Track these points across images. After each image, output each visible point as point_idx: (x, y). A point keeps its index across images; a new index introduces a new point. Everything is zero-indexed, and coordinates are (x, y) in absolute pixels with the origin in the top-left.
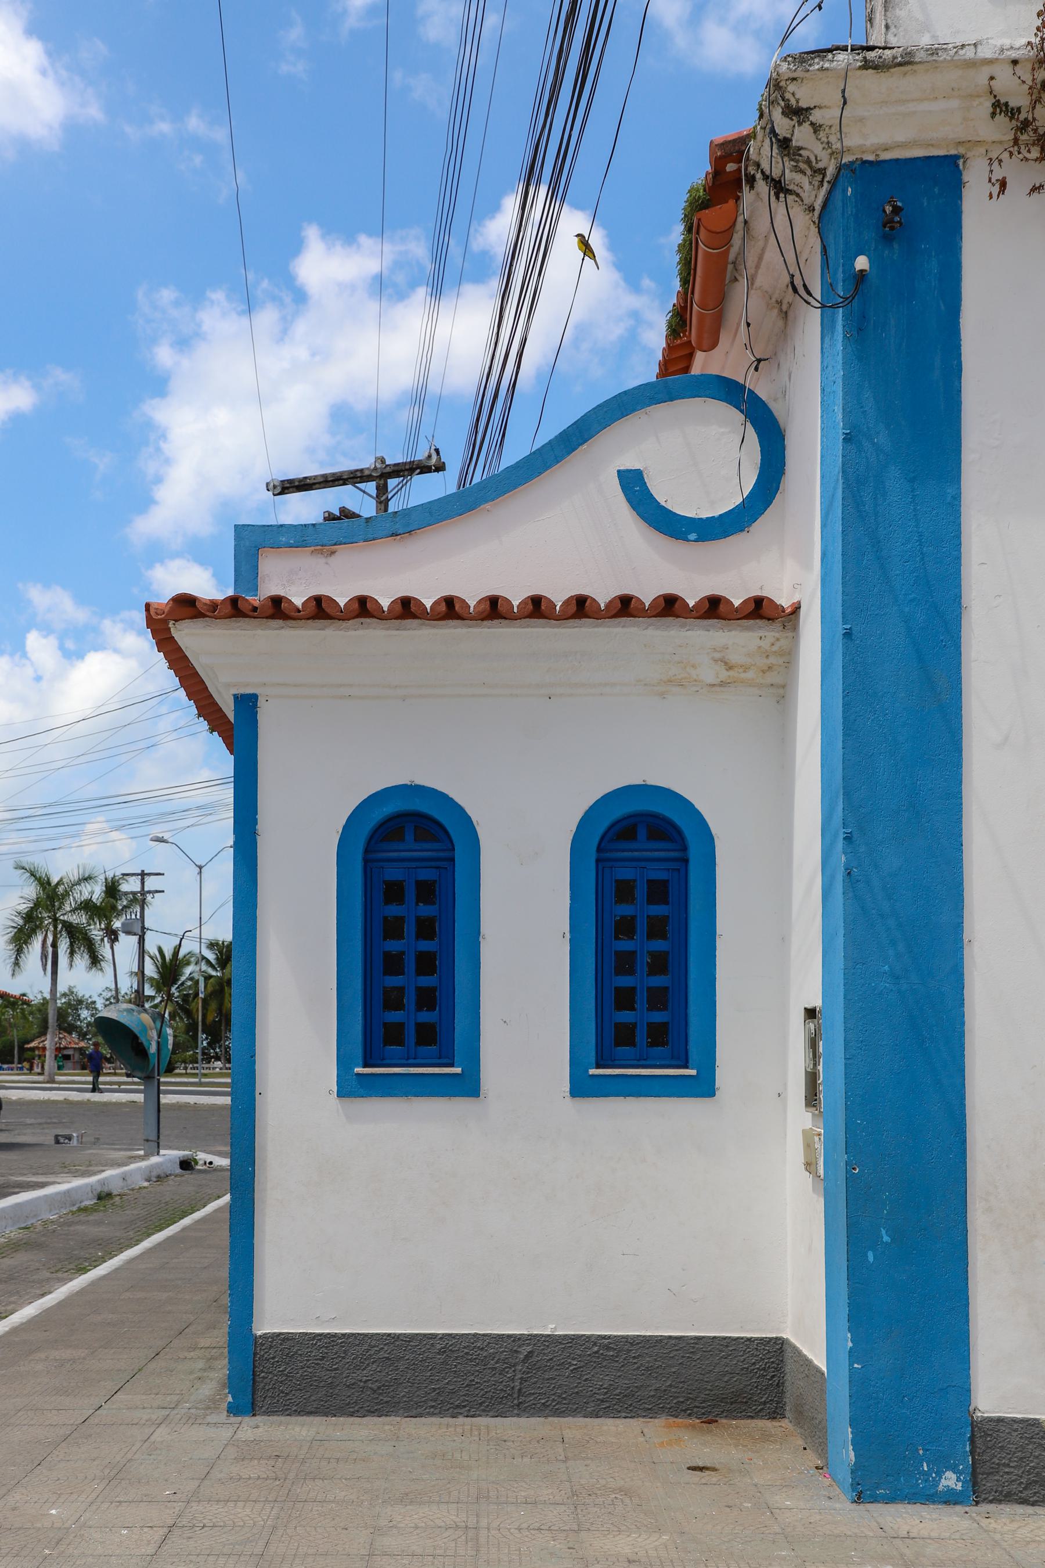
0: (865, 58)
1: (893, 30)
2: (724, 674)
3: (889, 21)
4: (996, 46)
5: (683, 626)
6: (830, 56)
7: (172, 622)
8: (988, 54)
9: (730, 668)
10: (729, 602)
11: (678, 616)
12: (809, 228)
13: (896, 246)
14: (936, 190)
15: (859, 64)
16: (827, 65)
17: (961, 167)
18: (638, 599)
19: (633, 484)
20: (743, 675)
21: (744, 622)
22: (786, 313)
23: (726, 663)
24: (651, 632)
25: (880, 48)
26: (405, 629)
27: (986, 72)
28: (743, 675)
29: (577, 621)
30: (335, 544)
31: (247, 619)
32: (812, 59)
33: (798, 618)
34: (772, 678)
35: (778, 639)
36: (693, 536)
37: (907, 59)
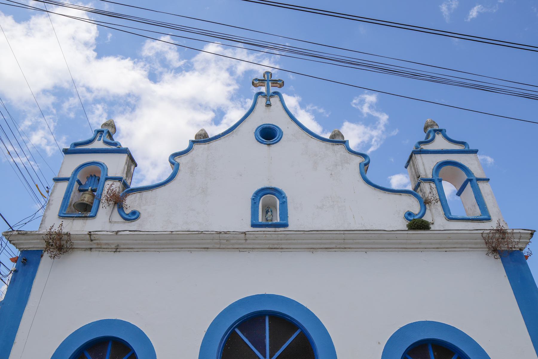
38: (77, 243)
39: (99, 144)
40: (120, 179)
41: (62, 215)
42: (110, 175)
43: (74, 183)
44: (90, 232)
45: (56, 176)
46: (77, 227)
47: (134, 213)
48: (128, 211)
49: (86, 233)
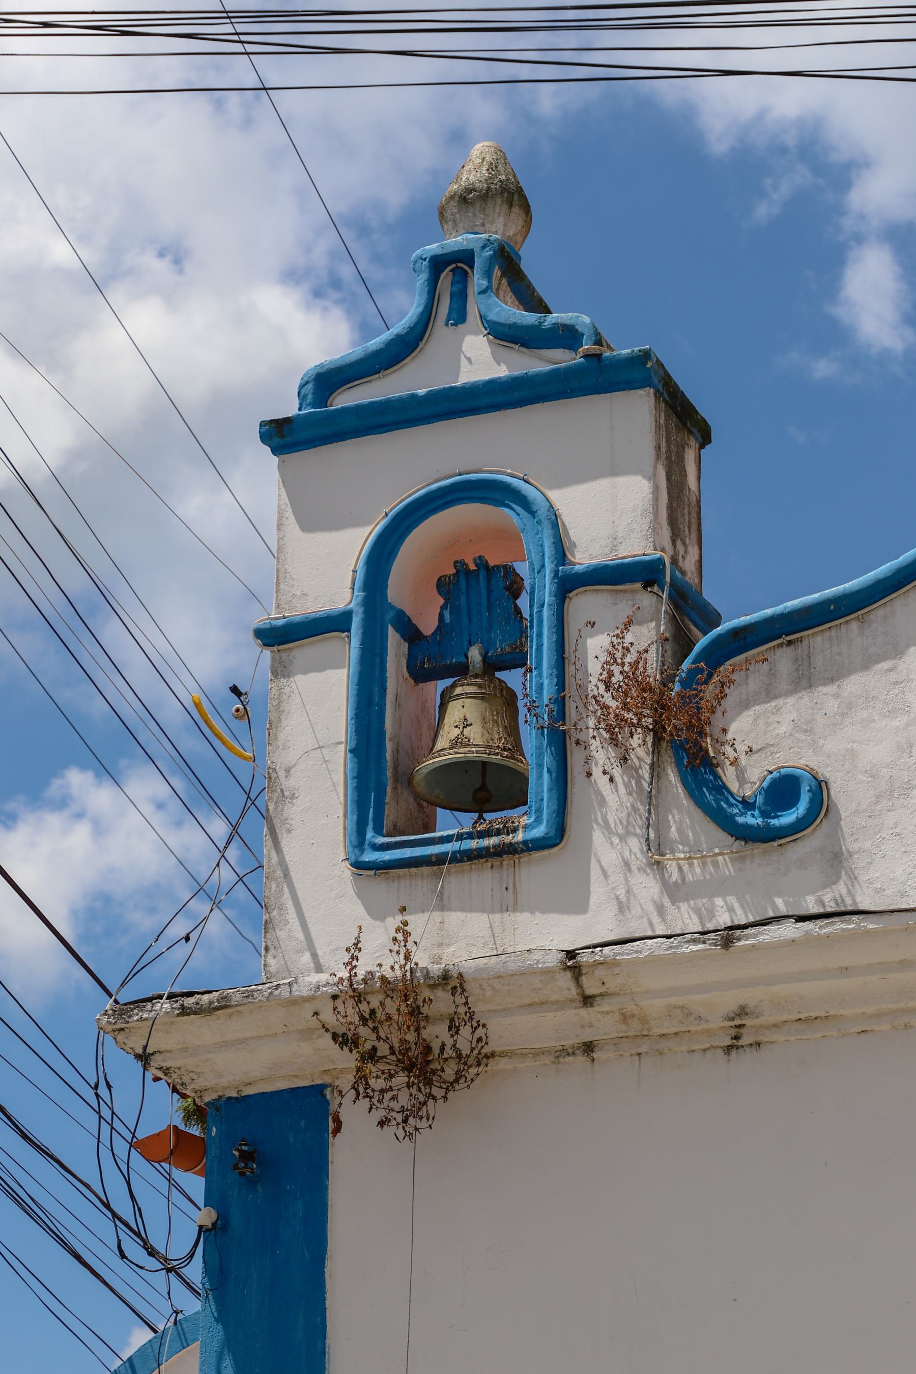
0: (182, 1005)
1: (272, 951)
3: (269, 943)
4: (311, 983)
6: (149, 1005)
8: (305, 993)
13: (260, 1188)
14: (303, 1123)
15: (177, 1012)
16: (145, 1015)
17: (328, 1097)
25: (198, 993)
27: (309, 1008)
32: (132, 1010)
37: (223, 1003)
38: (503, 1031)
39: (477, 359)
40: (645, 574)
41: (370, 856)
42: (587, 554)
43: (384, 637)
44: (571, 954)
45: (272, 614)
46: (470, 934)
47: (783, 789)
48: (747, 776)
49: (553, 960)
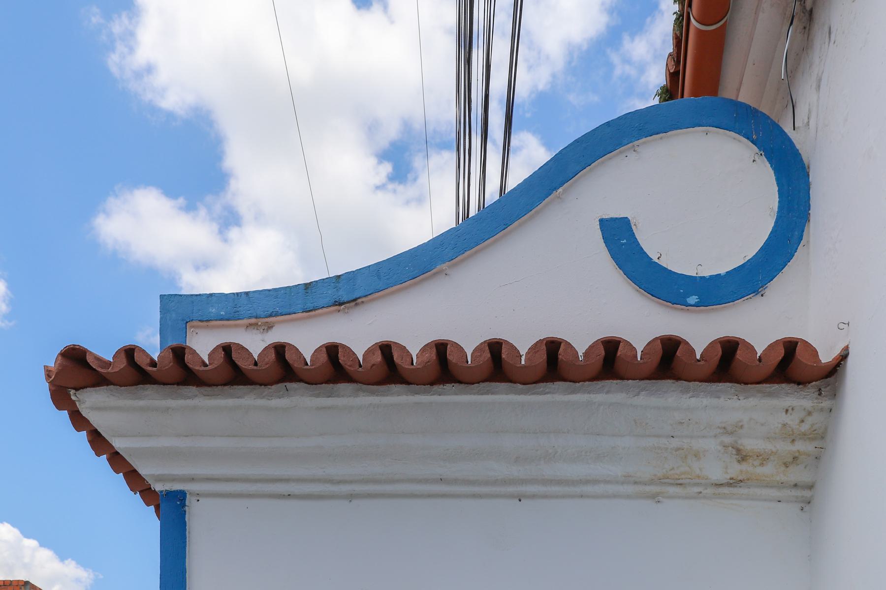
2: (736, 470)
5: (686, 391)
7: (72, 392)
9: (742, 457)
10: (751, 348)
11: (678, 378)
12: (701, 469)
18: (628, 344)
19: (618, 236)
20: (760, 470)
21: (766, 387)
22: (811, 11)
23: (738, 451)
24: (643, 399)
26: (338, 396)
28: (760, 470)
29: (549, 385)
30: (271, 316)
31: (155, 386)
33: (841, 381)
34: (797, 474)
35: (810, 413)
36: (693, 300)
